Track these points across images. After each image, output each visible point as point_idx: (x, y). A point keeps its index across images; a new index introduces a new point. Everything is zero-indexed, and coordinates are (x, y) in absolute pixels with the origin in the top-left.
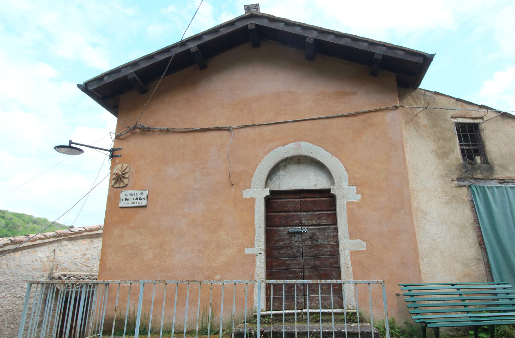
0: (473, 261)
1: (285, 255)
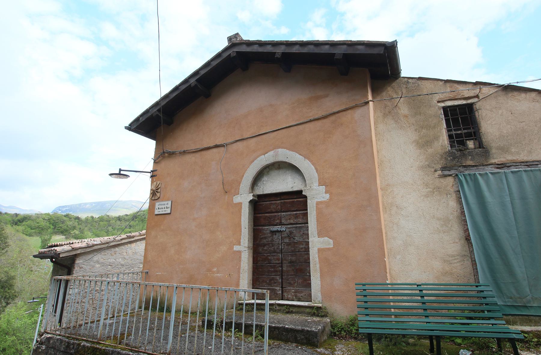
0: (456, 258)
1: (268, 251)
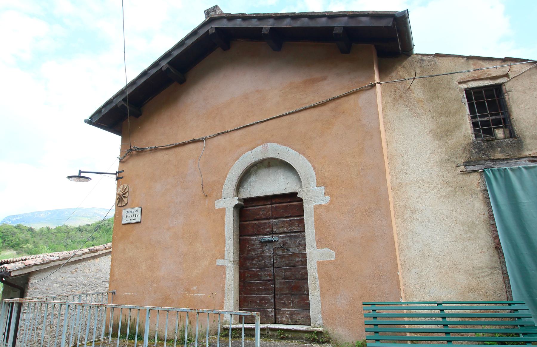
0: (484, 270)
1: (257, 266)
